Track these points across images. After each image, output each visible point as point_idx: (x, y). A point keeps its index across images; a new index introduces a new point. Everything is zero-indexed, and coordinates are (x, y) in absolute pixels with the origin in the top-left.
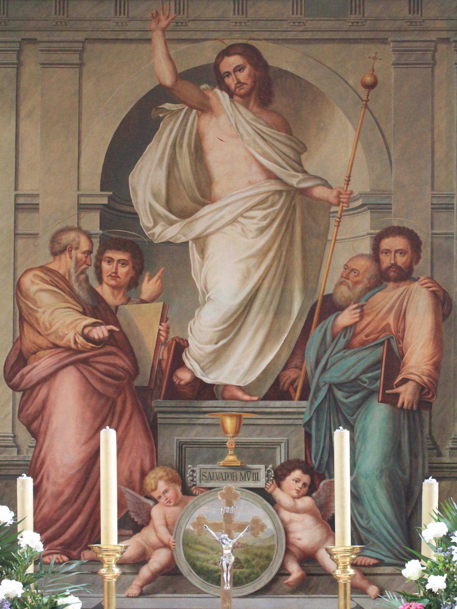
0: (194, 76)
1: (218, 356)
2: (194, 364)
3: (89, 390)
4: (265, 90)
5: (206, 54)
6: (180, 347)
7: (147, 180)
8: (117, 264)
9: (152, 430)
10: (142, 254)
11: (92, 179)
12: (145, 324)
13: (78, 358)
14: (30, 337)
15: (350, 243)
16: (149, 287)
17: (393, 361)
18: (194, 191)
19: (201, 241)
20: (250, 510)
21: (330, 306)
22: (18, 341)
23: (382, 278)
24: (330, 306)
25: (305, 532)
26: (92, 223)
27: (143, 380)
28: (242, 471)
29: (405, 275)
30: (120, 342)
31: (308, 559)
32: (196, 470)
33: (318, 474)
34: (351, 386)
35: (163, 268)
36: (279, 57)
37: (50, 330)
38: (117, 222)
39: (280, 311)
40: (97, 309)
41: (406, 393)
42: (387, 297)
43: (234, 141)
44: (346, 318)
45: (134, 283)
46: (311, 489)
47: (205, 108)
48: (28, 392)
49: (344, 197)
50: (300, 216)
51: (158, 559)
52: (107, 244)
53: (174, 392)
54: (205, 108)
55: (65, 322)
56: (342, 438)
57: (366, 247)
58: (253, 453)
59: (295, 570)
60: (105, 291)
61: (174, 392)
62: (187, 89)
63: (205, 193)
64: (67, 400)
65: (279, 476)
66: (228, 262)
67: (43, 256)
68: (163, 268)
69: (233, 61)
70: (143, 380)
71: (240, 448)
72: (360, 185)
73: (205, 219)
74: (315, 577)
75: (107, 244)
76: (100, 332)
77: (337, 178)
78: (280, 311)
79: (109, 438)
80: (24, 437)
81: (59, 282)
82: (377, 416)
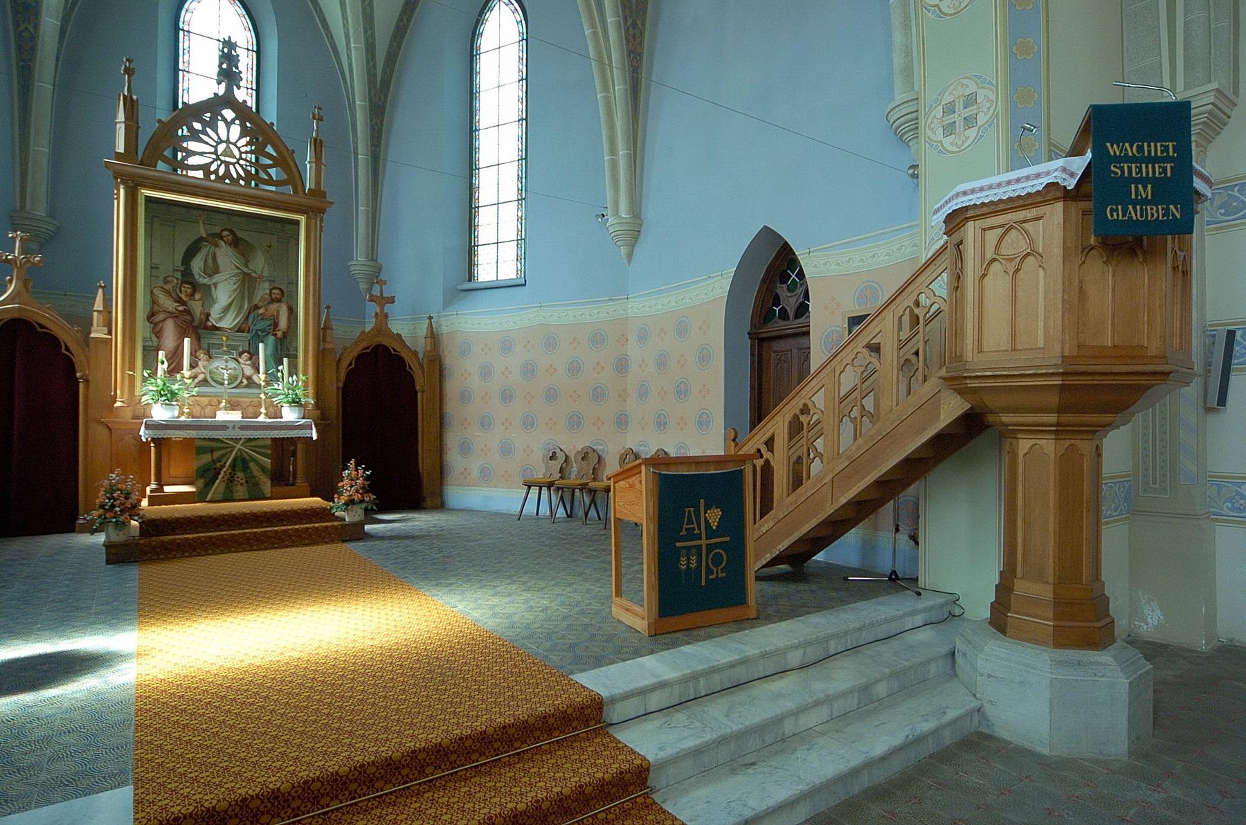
0: (214, 235)
1: (220, 319)
2: (212, 321)
3: (177, 326)
4: (236, 243)
5: (217, 230)
6: (208, 315)
7: (197, 264)
8: (187, 288)
9: (199, 339)
10: (195, 287)
11: (178, 262)
12: (197, 307)
13: (174, 315)
14: (156, 308)
15: (263, 290)
16: (197, 296)
17: (276, 325)
18: (213, 269)
19: (215, 285)
20: (232, 364)
21: (256, 307)
22: (152, 309)
23: (272, 301)
24: (256, 307)
25: (249, 371)
26: (179, 275)
27: (196, 323)
28: (228, 353)
29: (279, 301)
30: (188, 312)
31: (249, 378)
32: (213, 351)
33: (253, 355)
34: (263, 330)
35: (728, 539)
36: (239, 234)
37: (193, 320)
38: (187, 276)
39: (241, 308)
40: (180, 301)
41: (279, 334)
42: (274, 306)
43: (226, 257)
44: (261, 311)
45: (193, 295)
46: (250, 359)
47: (216, 245)
48: (156, 324)
49: (261, 277)
50: (247, 282)
51: (201, 377)
52: (183, 282)
53: (206, 328)
54: (216, 245)
55: (170, 305)
56: (261, 345)
57: (267, 292)
58: (231, 348)
59: (245, 382)
60: (183, 297)
61: (206, 328)
62: (210, 239)
63: (216, 270)
64: (170, 329)
65: (240, 354)
66: (224, 293)
67: (161, 284)
68: (728, 539)
69: (226, 233)
70: (196, 323)
71: (228, 346)
72: (266, 274)
73: (216, 278)
74: (251, 383)
75: (183, 282)
76: (181, 308)
77: (259, 270)
78: (241, 308)
79: (187, 341)
80: (154, 338)
81: (167, 292)
82: (271, 339)
